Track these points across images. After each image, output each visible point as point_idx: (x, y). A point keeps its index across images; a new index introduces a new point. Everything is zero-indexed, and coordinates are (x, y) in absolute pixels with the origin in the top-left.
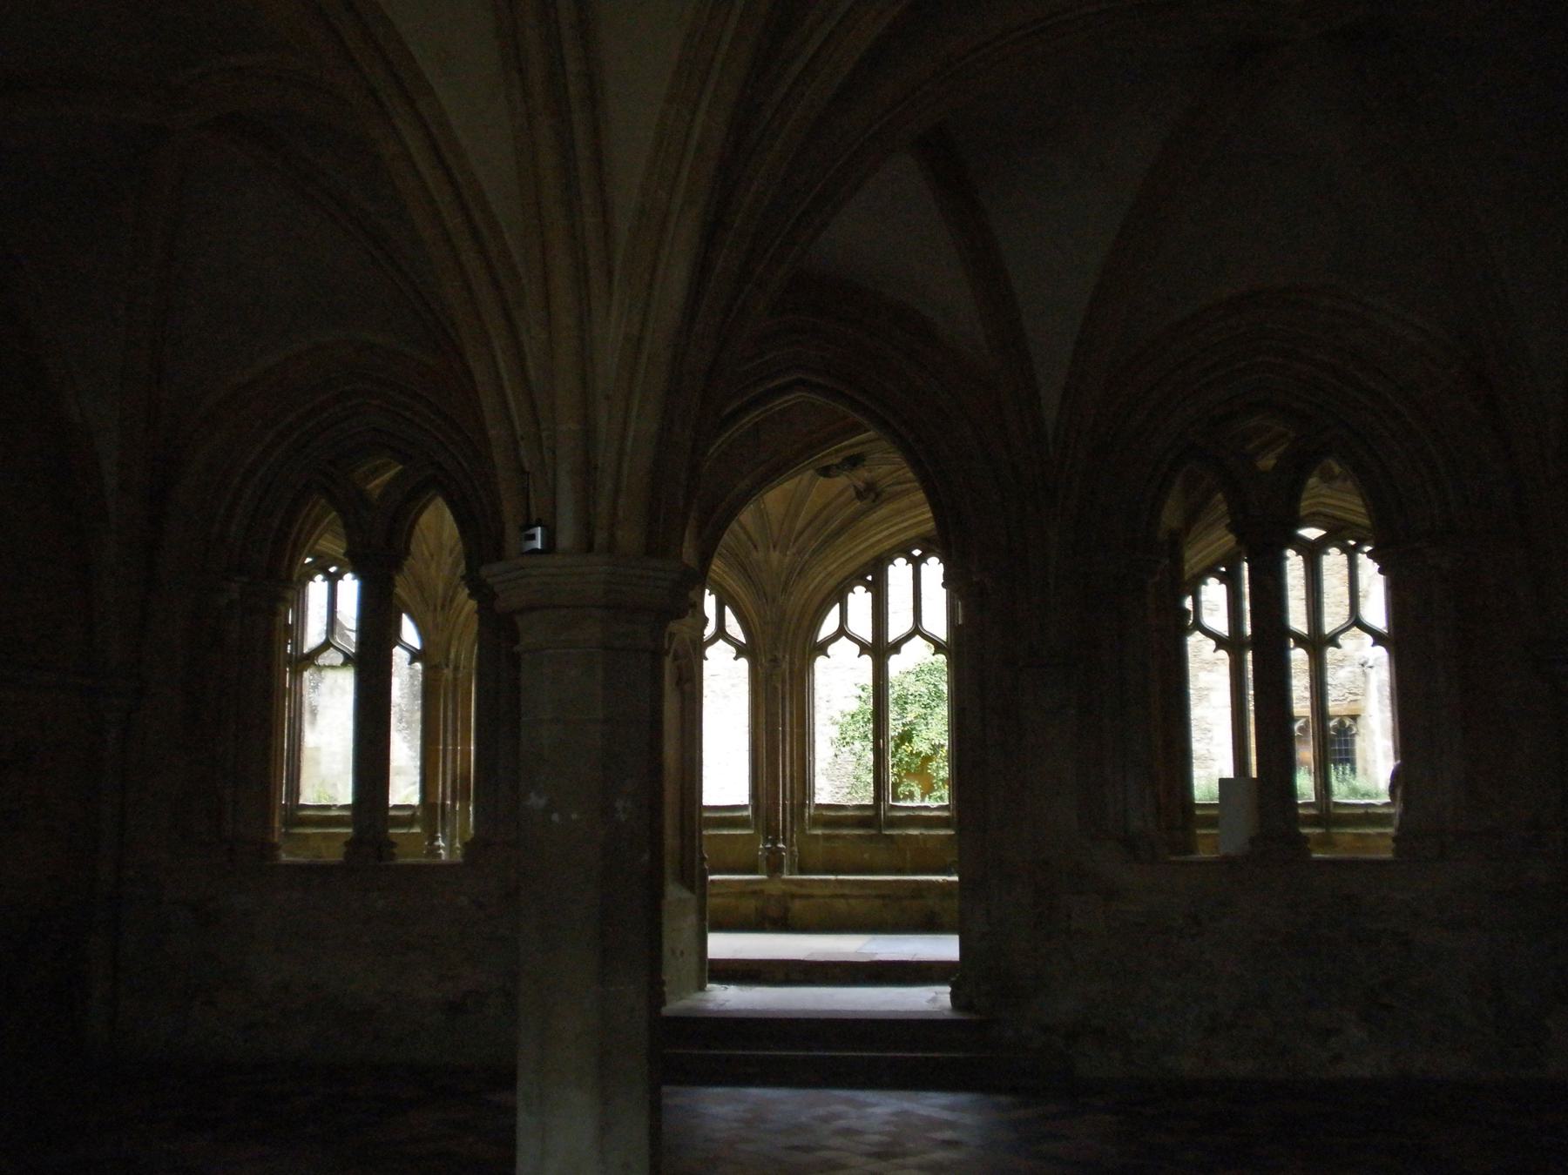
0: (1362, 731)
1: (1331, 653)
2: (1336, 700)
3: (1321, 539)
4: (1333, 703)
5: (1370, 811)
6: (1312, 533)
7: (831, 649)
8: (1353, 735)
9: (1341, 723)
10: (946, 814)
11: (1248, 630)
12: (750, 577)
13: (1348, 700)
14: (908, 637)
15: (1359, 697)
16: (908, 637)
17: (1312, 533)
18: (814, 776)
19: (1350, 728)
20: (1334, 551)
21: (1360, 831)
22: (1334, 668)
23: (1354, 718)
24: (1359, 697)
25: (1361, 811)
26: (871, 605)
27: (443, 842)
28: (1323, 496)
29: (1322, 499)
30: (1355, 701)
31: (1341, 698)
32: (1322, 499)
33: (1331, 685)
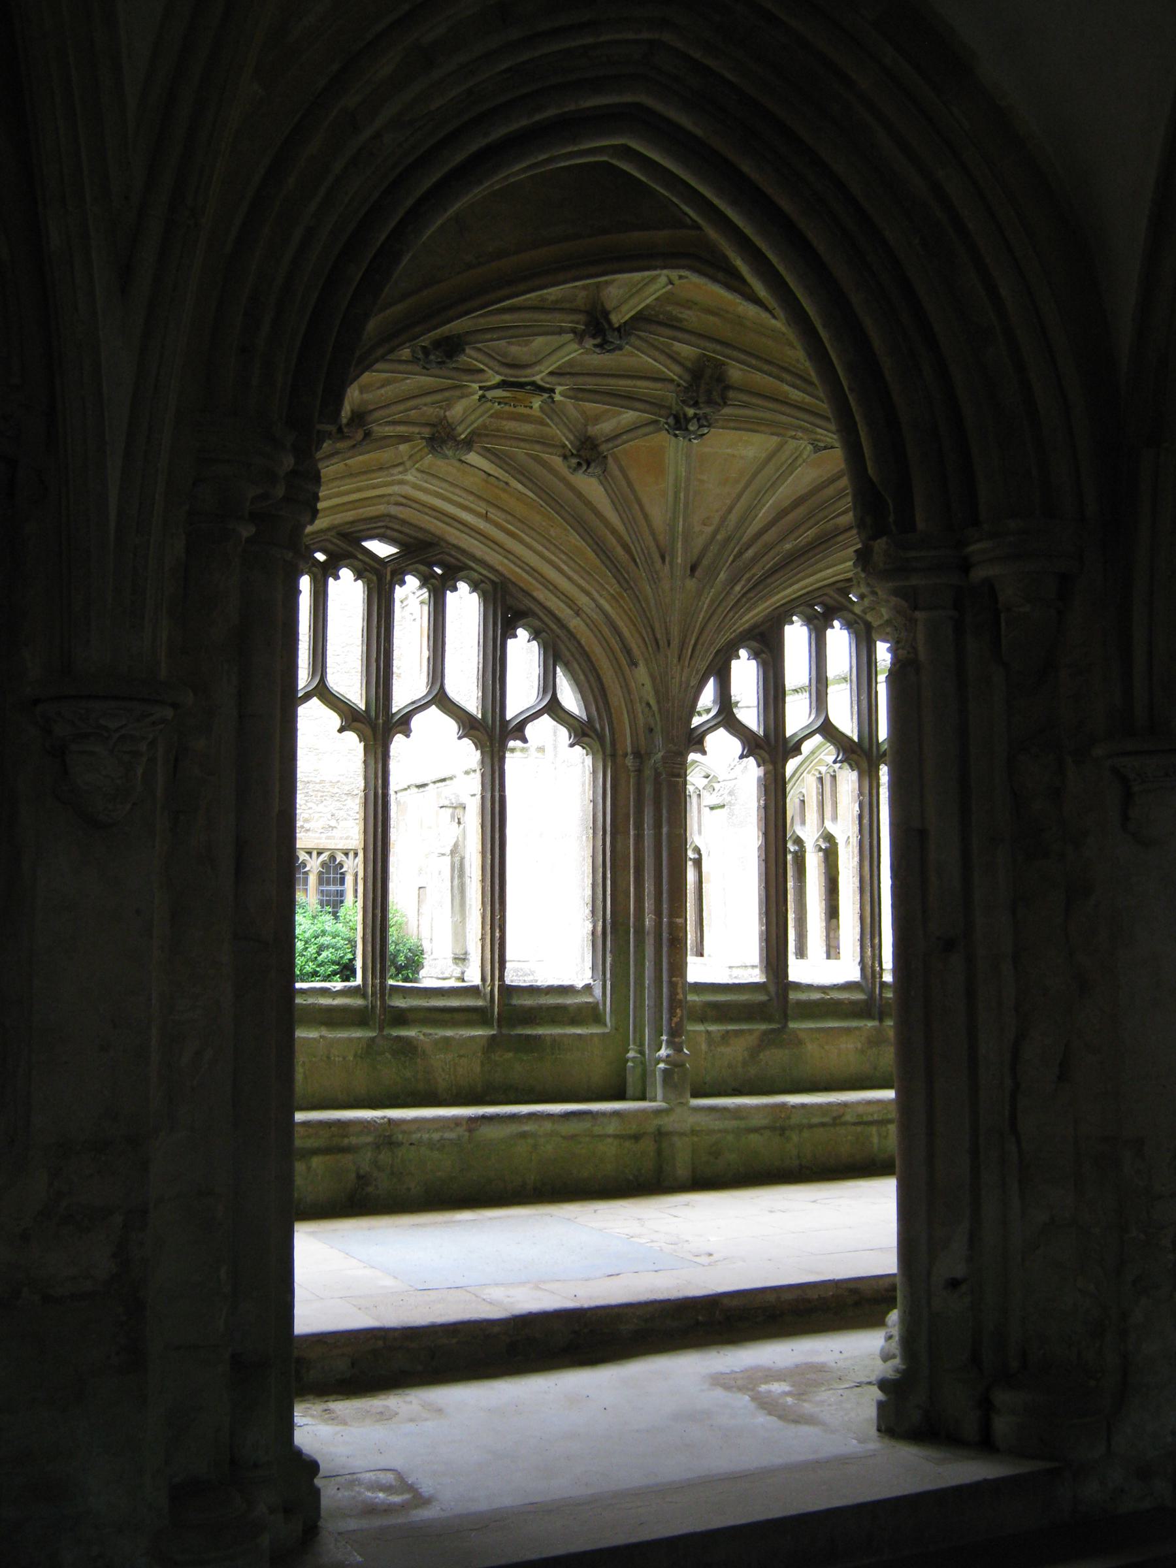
1: (398, 743)
3: (393, 559)
6: (381, 549)
7: (416, 722)
10: (358, 1002)
11: (883, 733)
12: (666, 629)
14: (419, 707)
16: (419, 707)
17: (381, 549)
18: (483, 939)
26: (732, 670)
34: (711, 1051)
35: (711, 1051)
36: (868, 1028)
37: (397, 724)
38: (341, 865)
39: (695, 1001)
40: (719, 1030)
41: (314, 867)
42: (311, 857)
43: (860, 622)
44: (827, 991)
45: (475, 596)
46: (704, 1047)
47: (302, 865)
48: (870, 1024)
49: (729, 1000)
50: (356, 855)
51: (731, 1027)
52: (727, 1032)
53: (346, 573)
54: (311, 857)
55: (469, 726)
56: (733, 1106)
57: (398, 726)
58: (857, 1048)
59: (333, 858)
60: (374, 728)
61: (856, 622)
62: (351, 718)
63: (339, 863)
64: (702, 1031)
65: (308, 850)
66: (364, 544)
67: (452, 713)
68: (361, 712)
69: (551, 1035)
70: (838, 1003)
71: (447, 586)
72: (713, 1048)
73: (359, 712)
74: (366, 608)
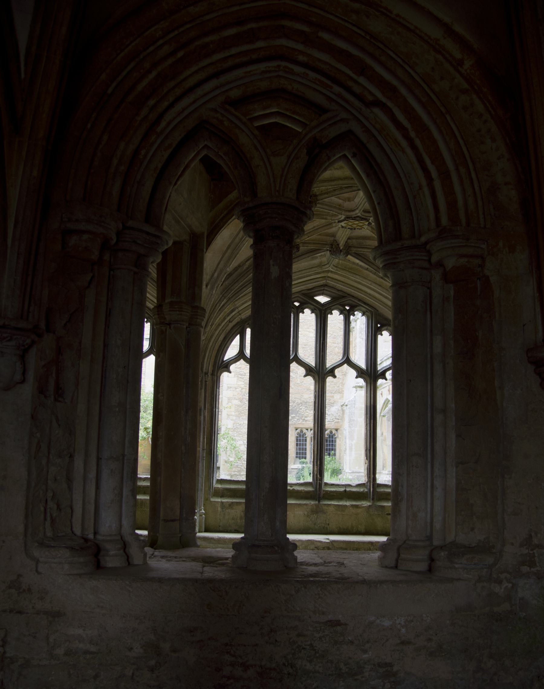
0: (340, 436)
1: (329, 380)
2: (329, 421)
4: (328, 423)
5: (348, 489)
6: (322, 299)
7: (232, 367)
8: (335, 438)
9: (331, 432)
13: (334, 422)
15: (339, 421)
17: (322, 299)
19: (334, 434)
20: (336, 313)
21: (341, 503)
22: (330, 407)
23: (337, 430)
24: (339, 421)
25: (342, 489)
27: (204, 510)
28: (332, 272)
29: (330, 275)
30: (338, 422)
31: (331, 421)
32: (330, 275)
33: (327, 414)
34: (223, 511)
35: (223, 511)
36: (311, 504)
37: (328, 373)
38: (305, 434)
39: (218, 487)
40: (228, 502)
41: (309, 435)
42: (308, 431)
43: (317, 309)
44: (292, 486)
45: (313, 315)
46: (219, 509)
47: (304, 434)
48: (313, 502)
49: (236, 488)
50: (311, 430)
51: (234, 500)
52: (232, 503)
53: (307, 311)
54: (308, 431)
55: (361, 373)
56: (217, 537)
57: (328, 374)
58: (304, 514)
59: (302, 431)
60: (370, 376)
61: (315, 309)
62: (309, 371)
63: (334, 434)
64: (219, 501)
65: (307, 429)
66: (315, 298)
67: (301, 365)
68: (313, 367)
69: (141, 499)
70: (298, 491)
71: (350, 314)
72: (224, 510)
73: (312, 367)
74: (367, 325)
